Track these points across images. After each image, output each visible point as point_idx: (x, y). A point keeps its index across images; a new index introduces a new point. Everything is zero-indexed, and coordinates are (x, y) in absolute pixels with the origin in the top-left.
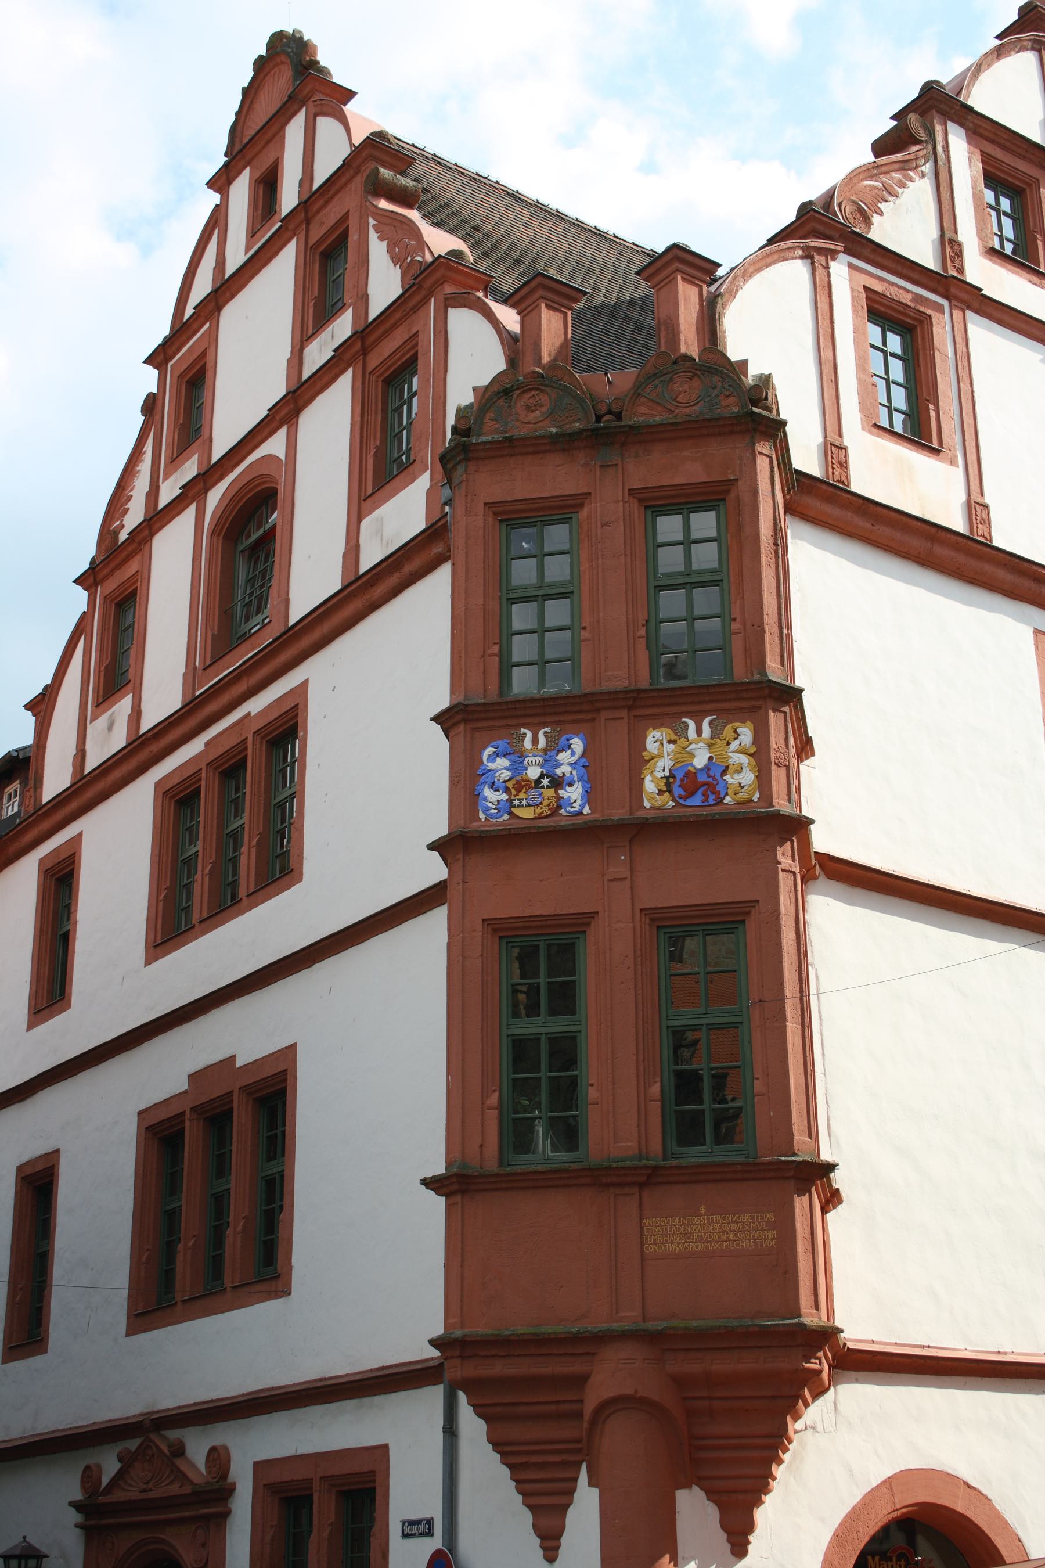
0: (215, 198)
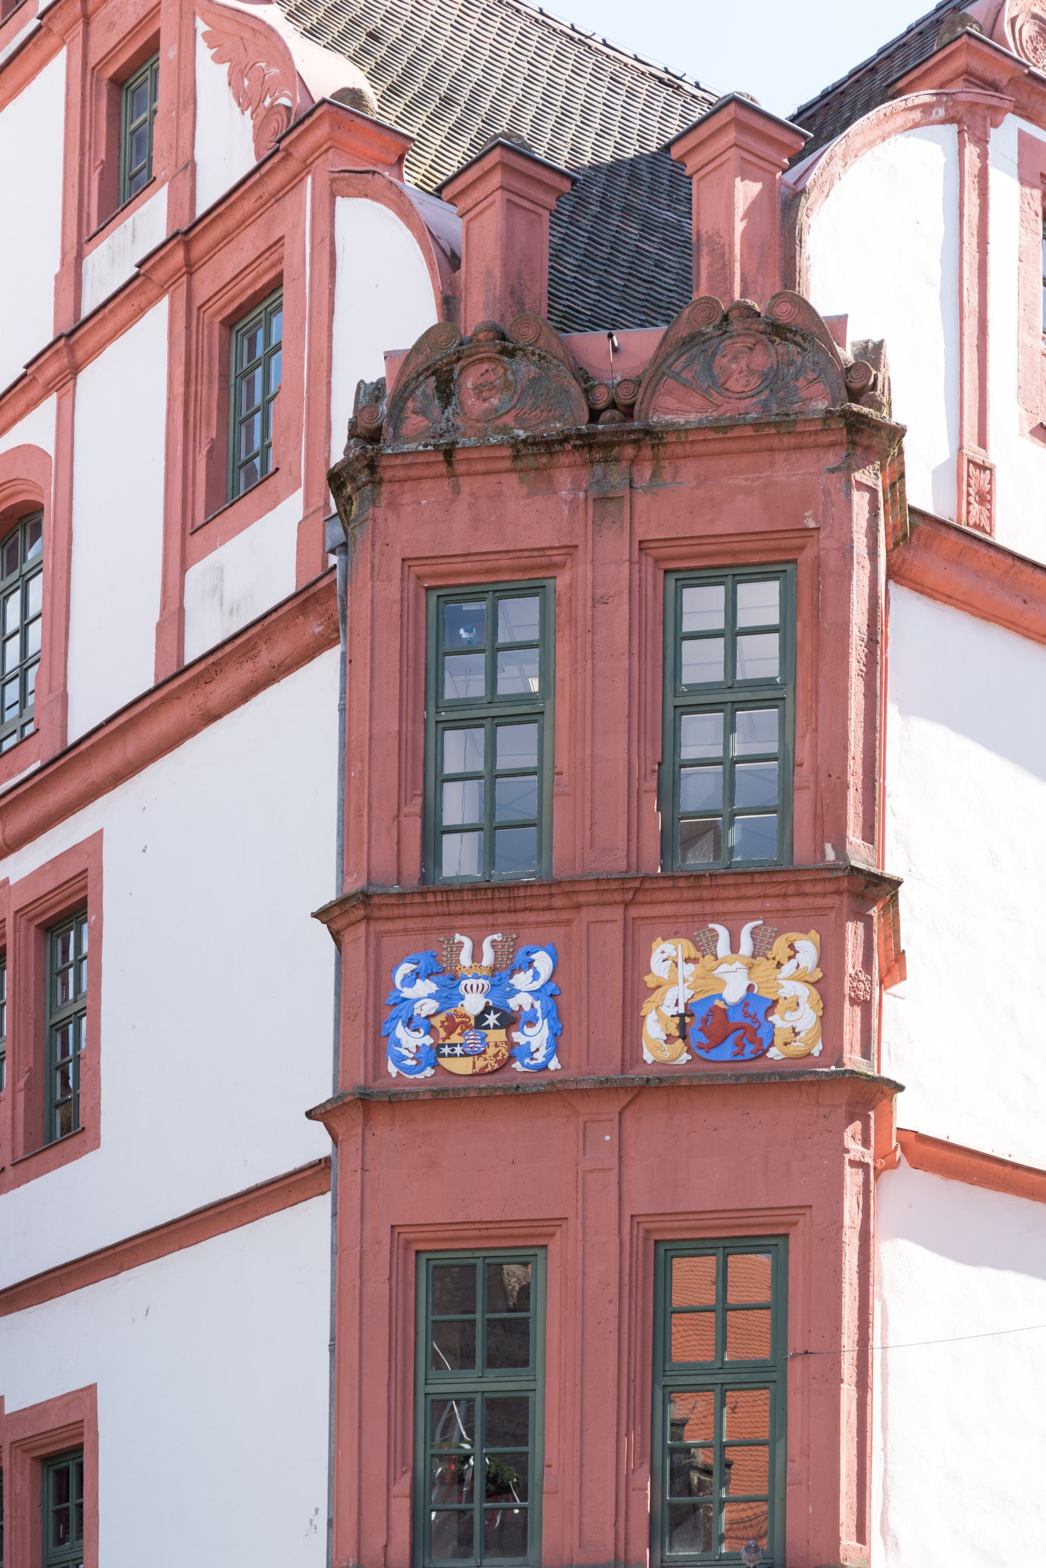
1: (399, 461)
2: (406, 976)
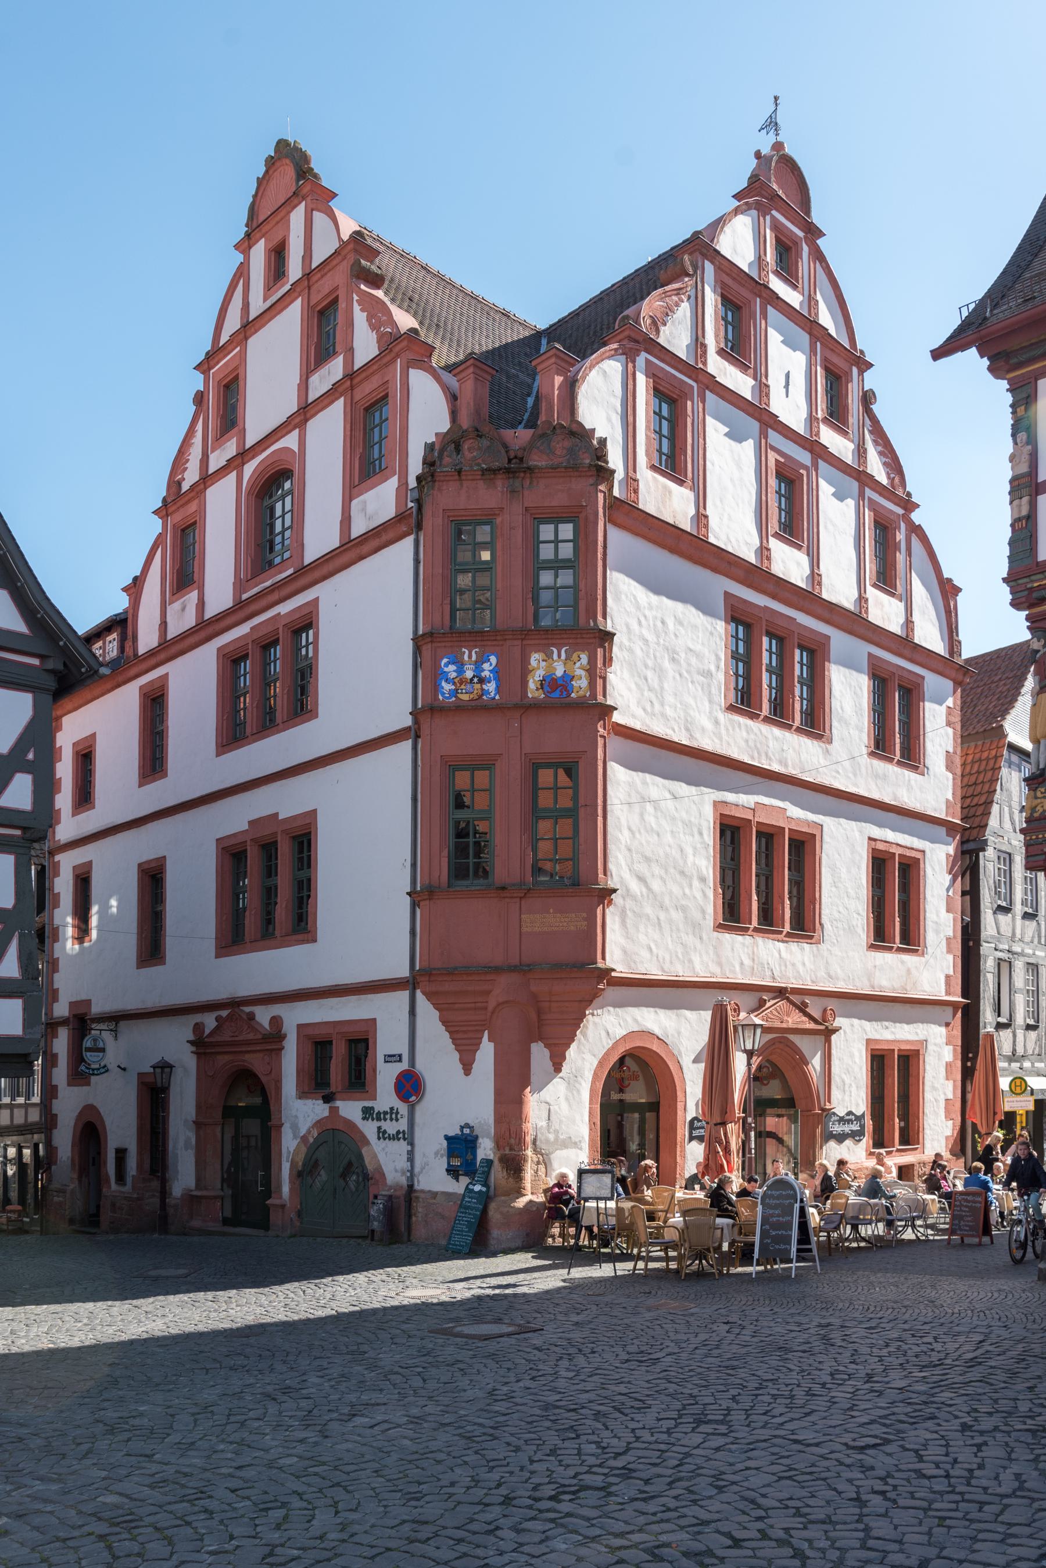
0: (240, 258)
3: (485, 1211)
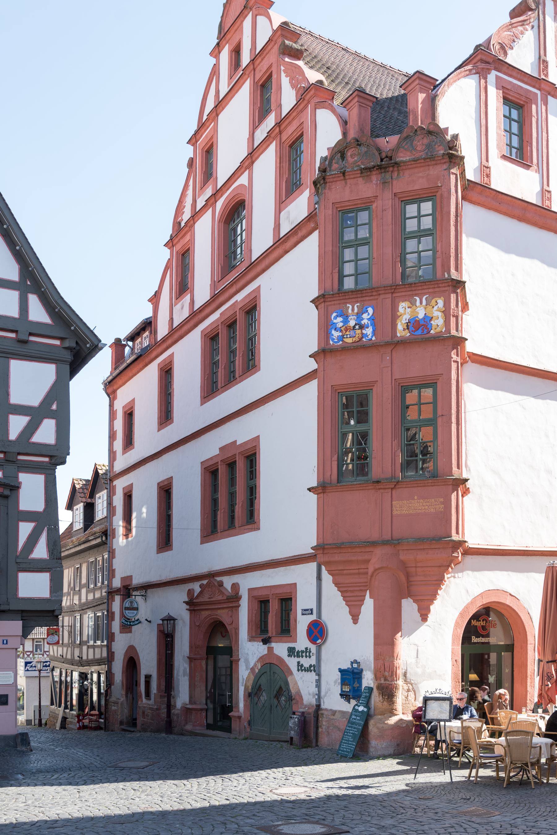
0: (213, 61)
1: (331, 177)
2: (334, 317)
3: (366, 726)
